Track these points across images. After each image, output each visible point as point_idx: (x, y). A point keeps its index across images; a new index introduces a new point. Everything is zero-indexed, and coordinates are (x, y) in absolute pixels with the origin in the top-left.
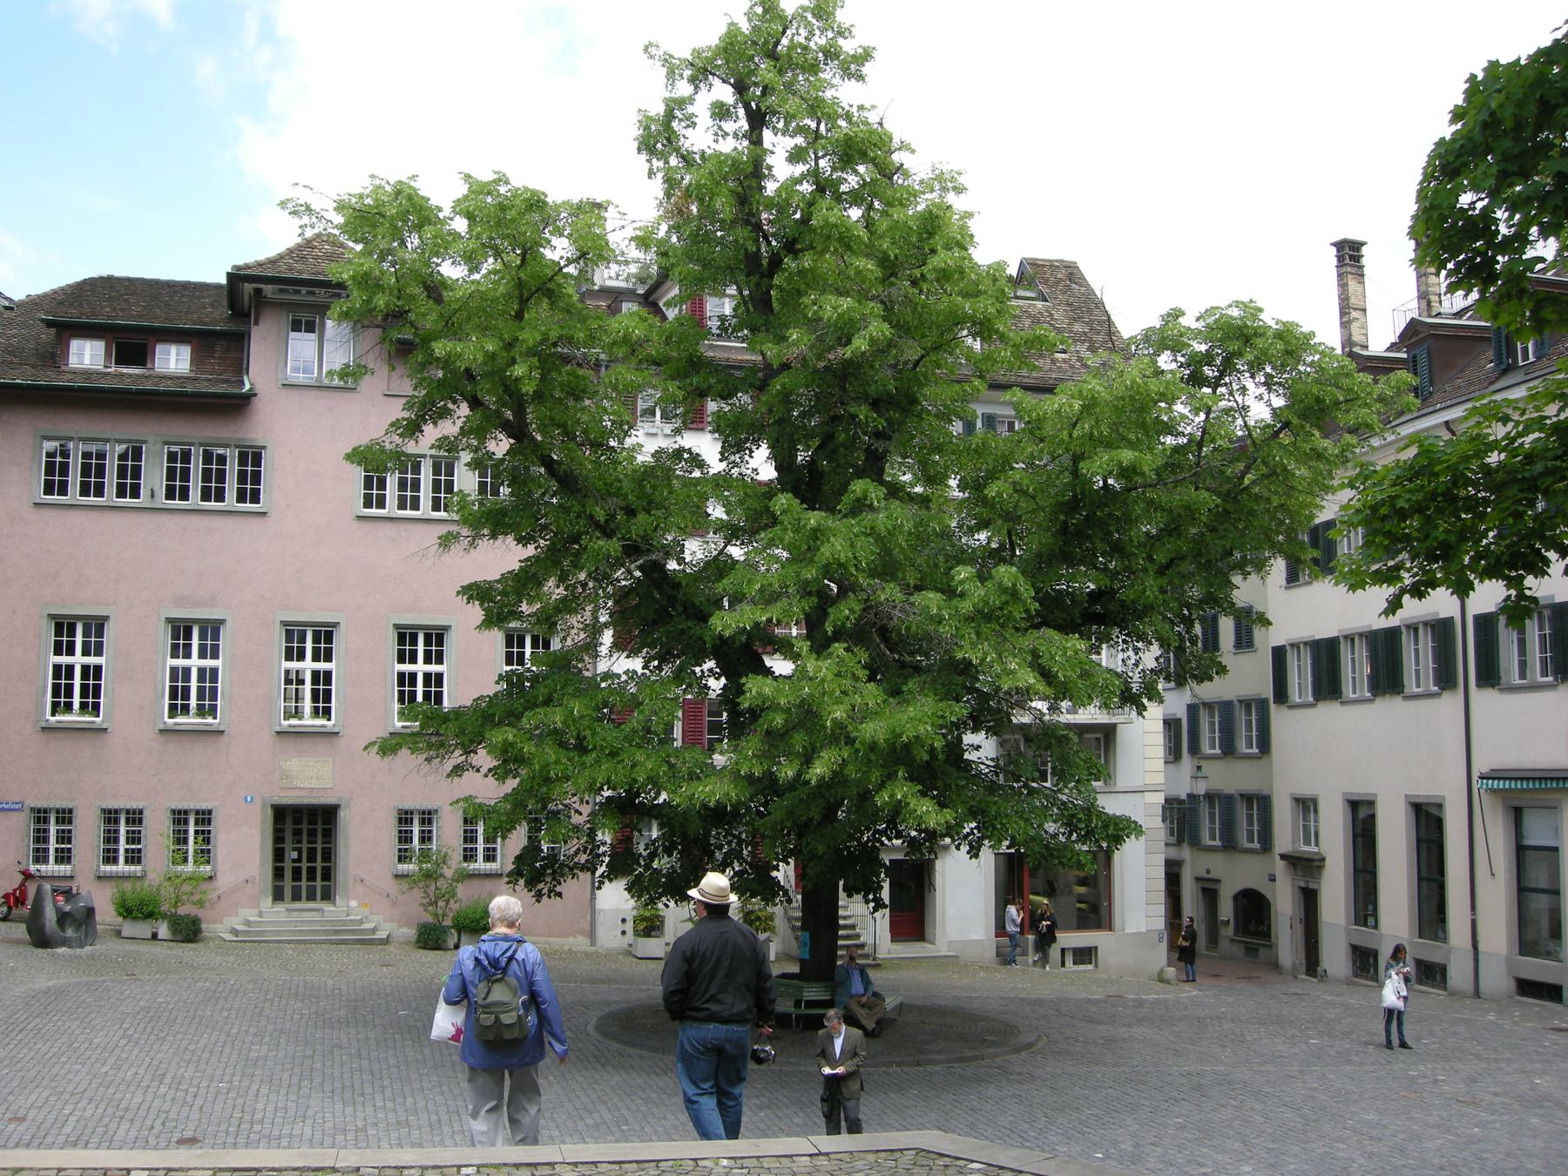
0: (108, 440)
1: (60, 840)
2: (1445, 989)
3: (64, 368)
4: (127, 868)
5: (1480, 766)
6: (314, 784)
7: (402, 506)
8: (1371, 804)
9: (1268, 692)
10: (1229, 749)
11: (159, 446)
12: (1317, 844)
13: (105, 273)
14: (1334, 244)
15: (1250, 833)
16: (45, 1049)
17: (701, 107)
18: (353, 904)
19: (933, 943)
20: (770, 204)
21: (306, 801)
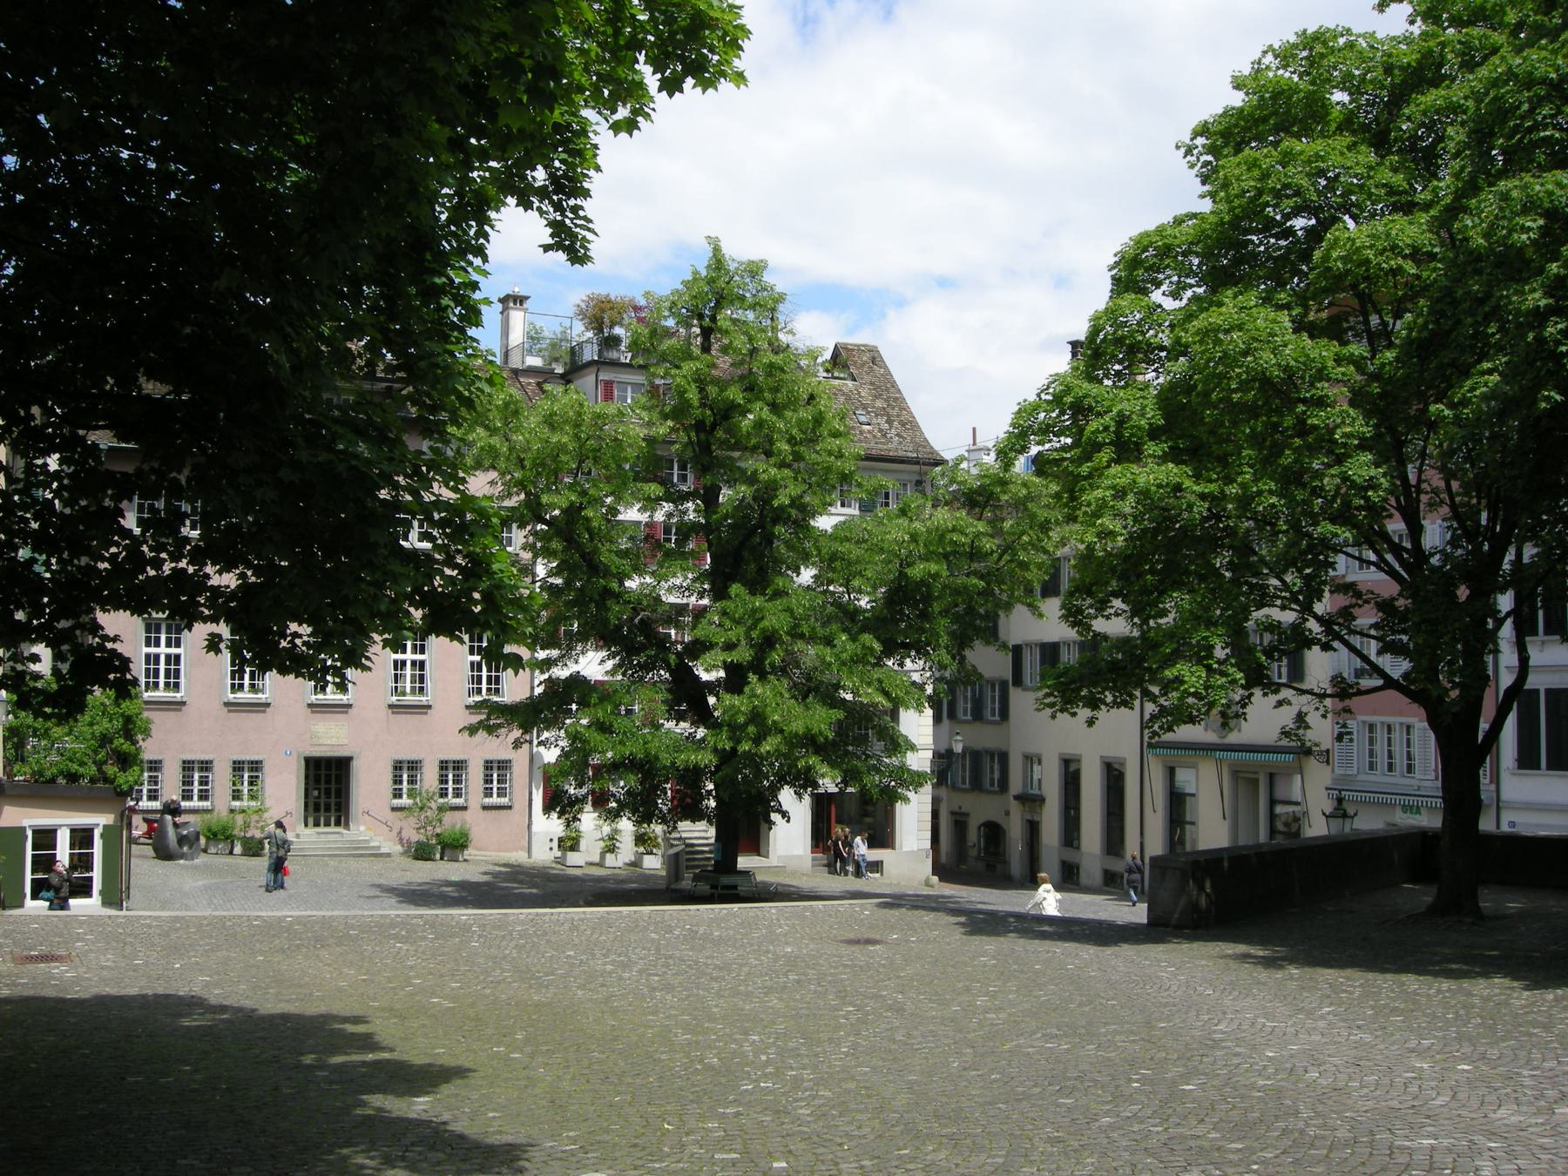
1: (201, 783)
4: (150, 803)
6: (334, 741)
9: (1008, 675)
14: (1070, 343)
15: (993, 710)
19: (767, 857)
21: (329, 754)
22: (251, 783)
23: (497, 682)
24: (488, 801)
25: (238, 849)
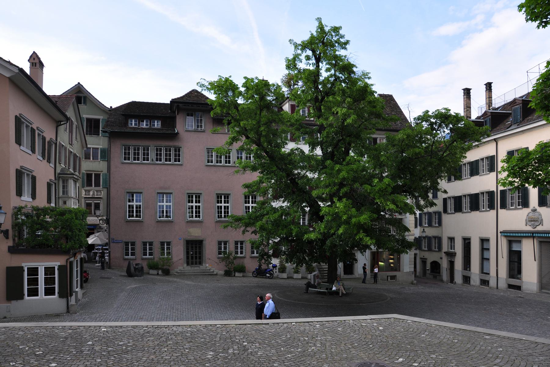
0: (140, 146)
2: (489, 287)
3: (128, 127)
5: (500, 229)
7: (226, 163)
8: (469, 239)
10: (430, 225)
11: (153, 148)
12: (454, 249)
14: (463, 89)
16: (141, 302)
17: (303, 57)
18: (207, 265)
20: (321, 83)
21: (194, 239)
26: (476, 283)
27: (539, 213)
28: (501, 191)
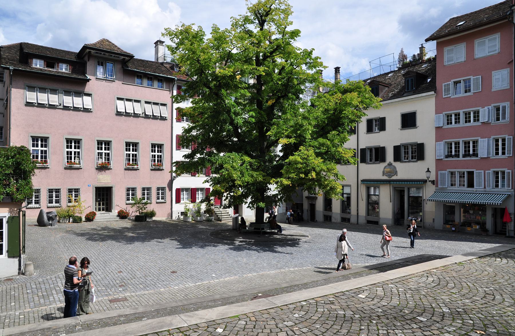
1: (56, 197)
5: (361, 178)
6: (106, 181)
13: (26, 42)
22: (75, 197)
23: (136, 161)
24: (158, 201)
25: (71, 220)
26: (337, 221)
27: (394, 166)
28: (361, 149)
